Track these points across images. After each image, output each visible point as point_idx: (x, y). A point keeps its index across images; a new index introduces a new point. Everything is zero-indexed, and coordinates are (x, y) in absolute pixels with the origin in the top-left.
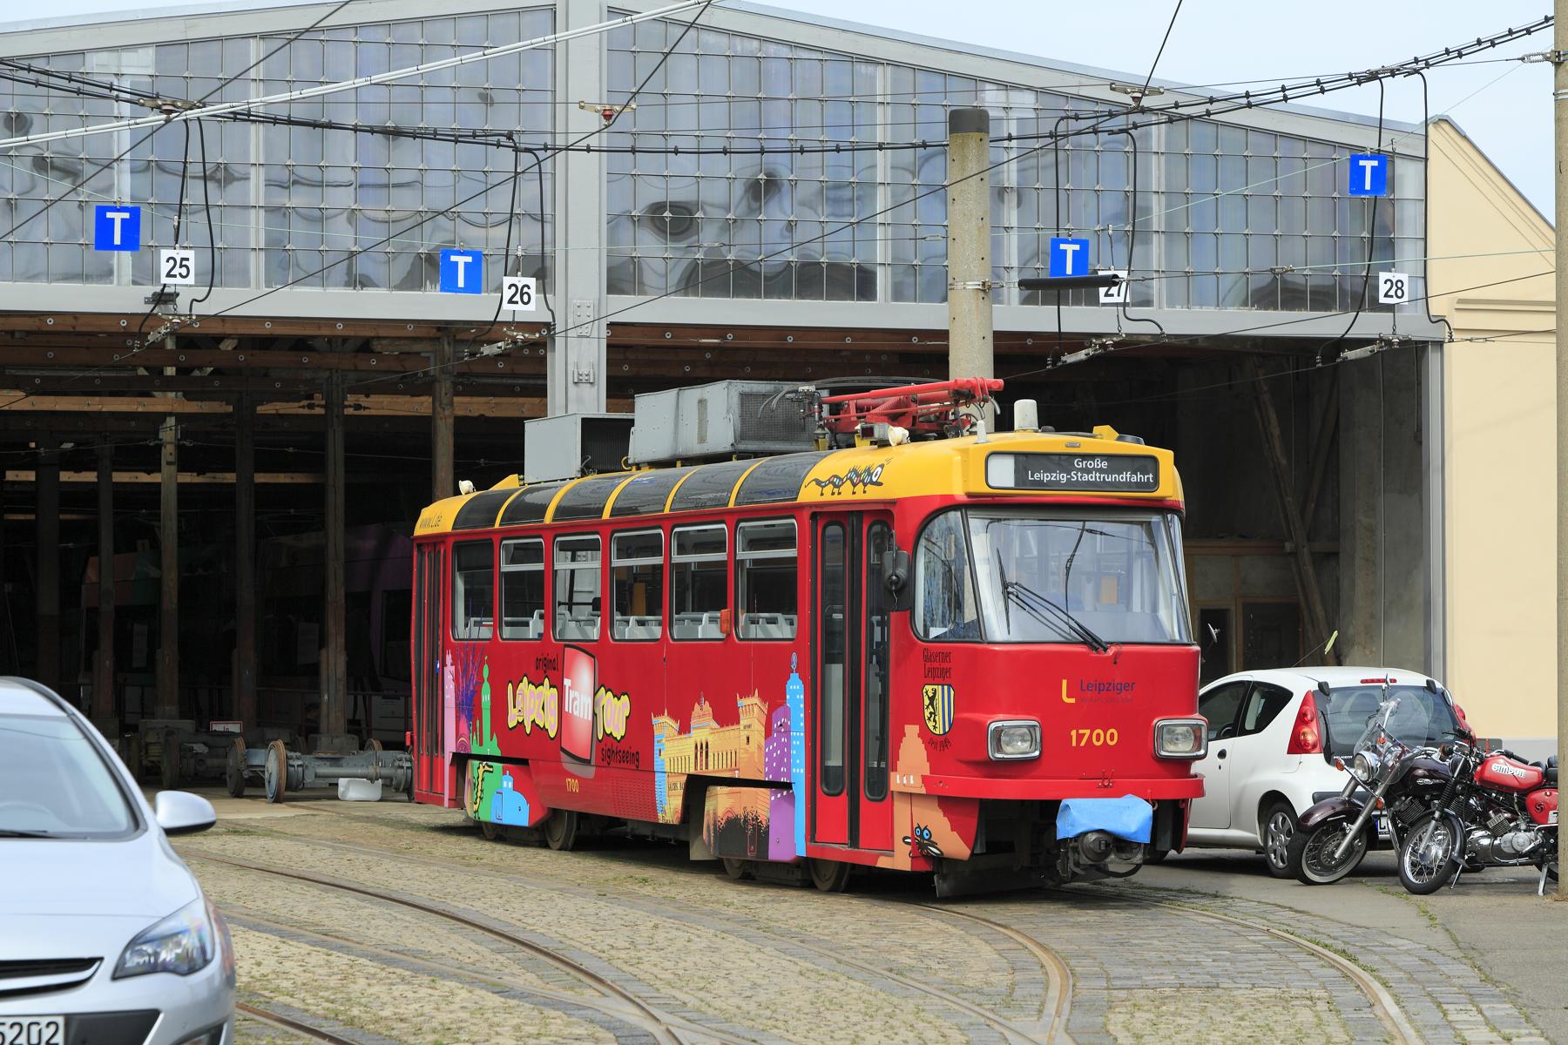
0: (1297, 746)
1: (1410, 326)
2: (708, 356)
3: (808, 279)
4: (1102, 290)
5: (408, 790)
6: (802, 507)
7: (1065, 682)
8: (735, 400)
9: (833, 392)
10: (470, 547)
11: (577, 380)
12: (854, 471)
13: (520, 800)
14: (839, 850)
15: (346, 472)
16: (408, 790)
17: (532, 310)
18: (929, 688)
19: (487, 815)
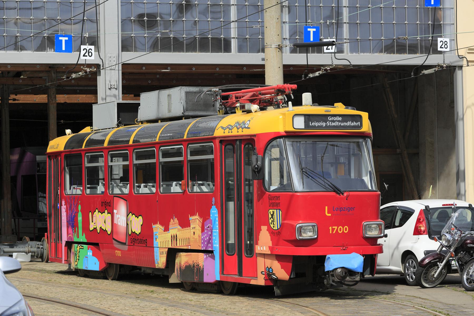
0: (417, 232)
1: (449, 59)
2: (158, 76)
3: (203, 44)
4: (325, 47)
5: (42, 257)
6: (215, 138)
7: (326, 207)
8: (183, 95)
9: (224, 91)
10: (71, 157)
11: (109, 87)
12: (238, 123)
13: (95, 260)
14: (234, 277)
15: (10, 126)
16: (42, 257)
17: (93, 59)
18: (271, 211)
19: (81, 266)
